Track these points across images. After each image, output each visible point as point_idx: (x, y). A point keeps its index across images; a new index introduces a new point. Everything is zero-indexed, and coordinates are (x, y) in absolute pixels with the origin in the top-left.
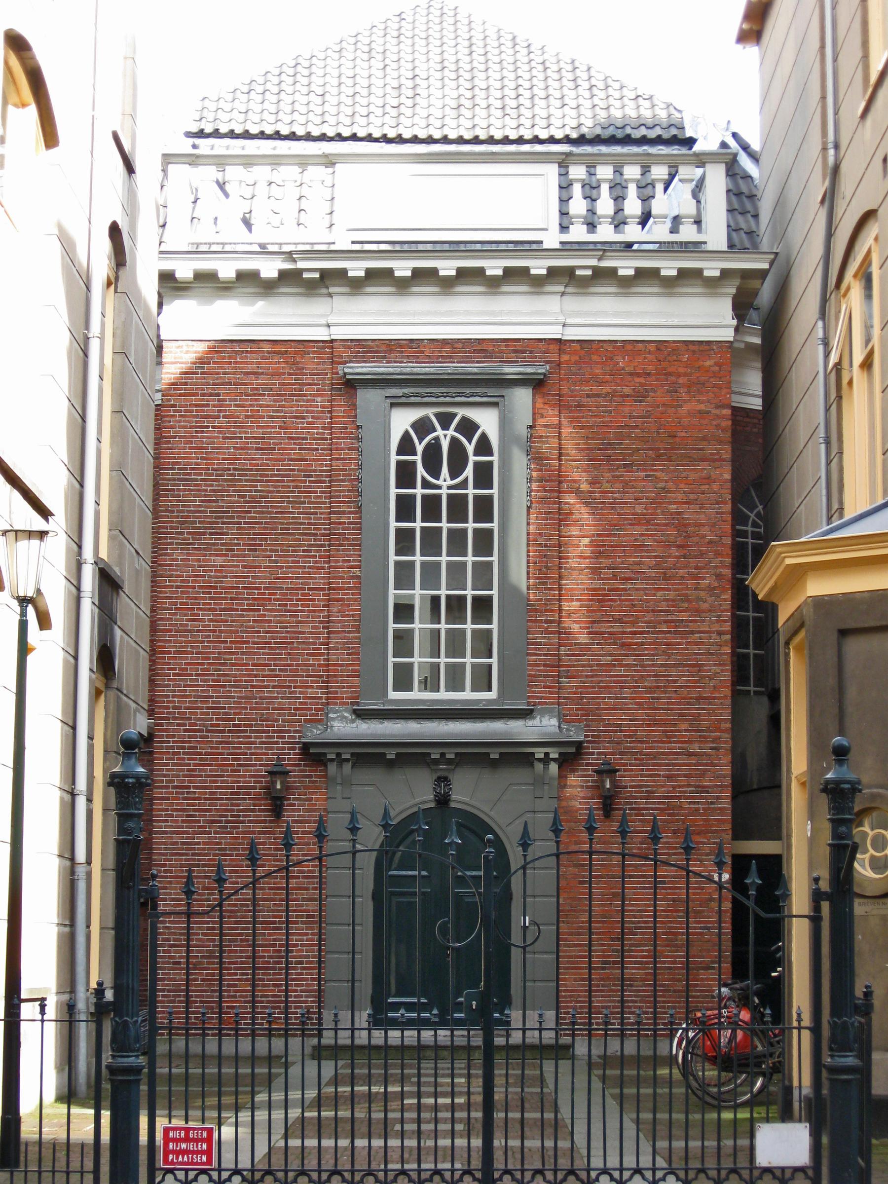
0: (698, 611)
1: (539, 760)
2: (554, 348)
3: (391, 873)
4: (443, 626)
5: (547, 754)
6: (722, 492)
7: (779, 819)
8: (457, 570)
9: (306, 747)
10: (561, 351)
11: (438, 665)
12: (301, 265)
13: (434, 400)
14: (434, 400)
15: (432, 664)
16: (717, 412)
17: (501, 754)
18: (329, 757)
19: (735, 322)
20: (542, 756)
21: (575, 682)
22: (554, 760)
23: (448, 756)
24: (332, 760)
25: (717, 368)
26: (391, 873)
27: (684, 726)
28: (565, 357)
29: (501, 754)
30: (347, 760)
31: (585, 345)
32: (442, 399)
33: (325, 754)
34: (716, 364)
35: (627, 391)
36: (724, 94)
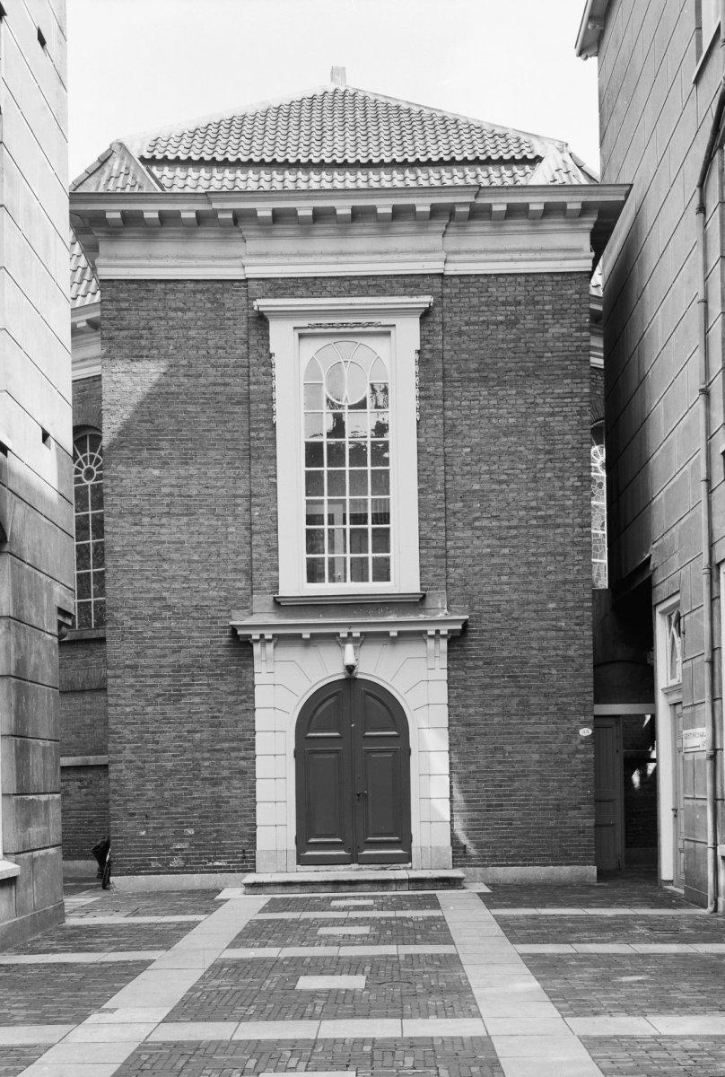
0: (563, 508)
1: (431, 637)
2: (437, 281)
3: (309, 735)
4: (326, 556)
5: (438, 632)
6: (583, 404)
7: (653, 679)
8: (359, 478)
9: (234, 629)
10: (444, 285)
11: (365, 523)
12: (216, 206)
13: (335, 330)
14: (335, 330)
15: (366, 516)
16: (578, 334)
17: (311, 634)
18: (254, 637)
19: (593, 254)
20: (433, 633)
21: (460, 571)
22: (444, 636)
23: (354, 635)
24: (257, 641)
25: (578, 296)
26: (309, 735)
27: (552, 606)
28: (447, 291)
29: (311, 634)
30: (269, 641)
31: (465, 280)
32: (342, 330)
33: (251, 636)
34: (577, 293)
35: (501, 318)
36: (554, 112)
